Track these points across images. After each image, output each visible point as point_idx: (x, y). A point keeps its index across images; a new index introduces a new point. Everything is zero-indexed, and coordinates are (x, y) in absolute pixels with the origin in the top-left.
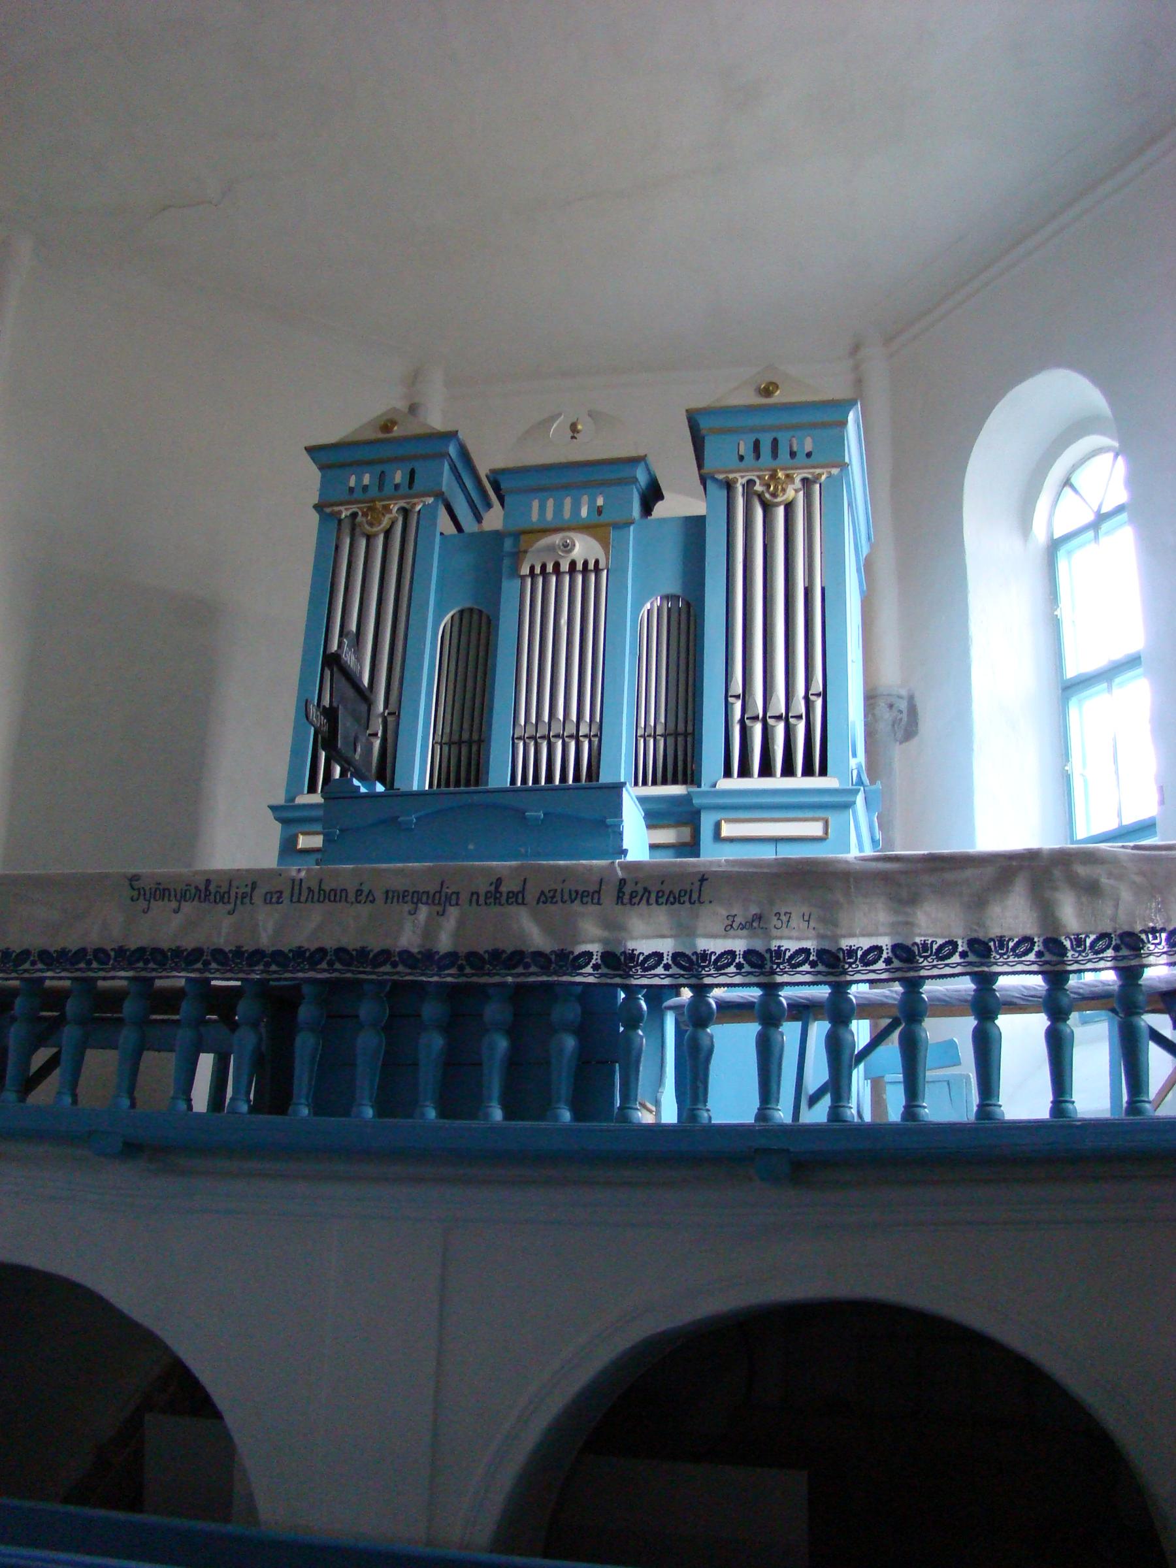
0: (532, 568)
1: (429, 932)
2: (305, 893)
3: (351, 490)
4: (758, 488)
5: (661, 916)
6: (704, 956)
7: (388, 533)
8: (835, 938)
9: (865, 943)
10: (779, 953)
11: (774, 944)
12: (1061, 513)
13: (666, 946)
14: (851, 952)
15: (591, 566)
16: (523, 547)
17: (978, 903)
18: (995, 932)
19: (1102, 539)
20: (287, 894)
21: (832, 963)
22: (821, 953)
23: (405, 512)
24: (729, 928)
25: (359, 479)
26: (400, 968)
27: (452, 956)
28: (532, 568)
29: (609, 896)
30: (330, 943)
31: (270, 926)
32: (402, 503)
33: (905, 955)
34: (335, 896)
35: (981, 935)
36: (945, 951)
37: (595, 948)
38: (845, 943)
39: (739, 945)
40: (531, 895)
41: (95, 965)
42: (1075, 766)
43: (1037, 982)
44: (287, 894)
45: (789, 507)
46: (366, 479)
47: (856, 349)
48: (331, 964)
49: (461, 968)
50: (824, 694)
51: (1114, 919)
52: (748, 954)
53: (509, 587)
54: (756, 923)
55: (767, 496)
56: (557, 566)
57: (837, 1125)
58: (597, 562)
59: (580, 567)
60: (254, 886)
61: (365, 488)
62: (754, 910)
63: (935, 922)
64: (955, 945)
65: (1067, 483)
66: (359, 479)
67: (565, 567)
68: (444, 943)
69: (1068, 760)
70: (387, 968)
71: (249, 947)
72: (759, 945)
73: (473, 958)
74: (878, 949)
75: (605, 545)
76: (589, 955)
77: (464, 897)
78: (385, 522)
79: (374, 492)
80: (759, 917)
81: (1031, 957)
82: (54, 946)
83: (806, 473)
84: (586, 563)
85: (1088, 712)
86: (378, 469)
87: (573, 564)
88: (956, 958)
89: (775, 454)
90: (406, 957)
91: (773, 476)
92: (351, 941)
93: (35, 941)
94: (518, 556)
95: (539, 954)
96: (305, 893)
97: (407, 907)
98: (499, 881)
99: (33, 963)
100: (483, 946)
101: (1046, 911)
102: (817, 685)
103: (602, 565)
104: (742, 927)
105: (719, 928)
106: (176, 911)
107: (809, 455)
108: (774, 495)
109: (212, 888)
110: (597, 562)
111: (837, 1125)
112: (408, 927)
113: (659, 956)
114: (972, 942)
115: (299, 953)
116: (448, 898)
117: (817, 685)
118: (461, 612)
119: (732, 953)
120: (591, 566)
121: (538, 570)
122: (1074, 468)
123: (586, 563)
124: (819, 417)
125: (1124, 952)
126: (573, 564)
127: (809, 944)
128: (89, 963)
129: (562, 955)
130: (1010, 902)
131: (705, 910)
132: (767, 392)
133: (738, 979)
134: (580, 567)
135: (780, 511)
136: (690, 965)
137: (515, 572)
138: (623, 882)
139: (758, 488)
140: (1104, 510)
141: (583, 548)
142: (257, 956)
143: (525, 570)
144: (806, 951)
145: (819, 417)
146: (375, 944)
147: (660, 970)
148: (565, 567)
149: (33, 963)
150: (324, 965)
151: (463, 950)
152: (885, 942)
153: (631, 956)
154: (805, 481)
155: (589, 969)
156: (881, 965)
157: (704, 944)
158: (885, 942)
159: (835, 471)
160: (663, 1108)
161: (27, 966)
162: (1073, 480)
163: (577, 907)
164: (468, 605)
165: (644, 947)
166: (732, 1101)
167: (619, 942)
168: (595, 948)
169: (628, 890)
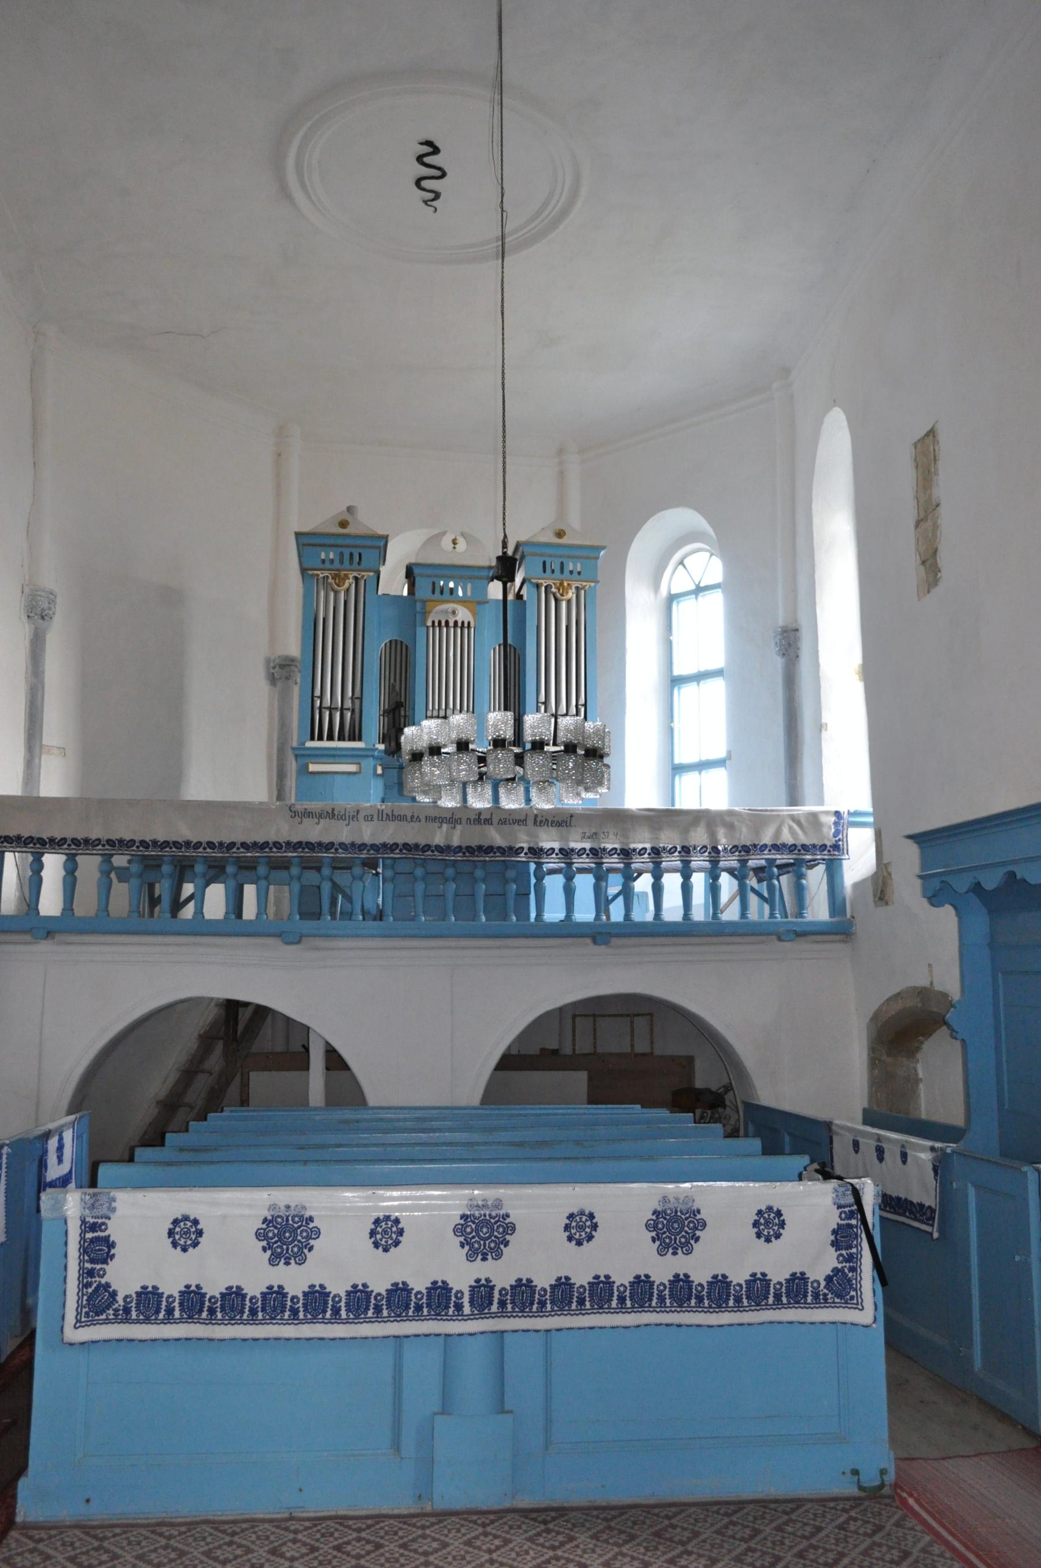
0: (433, 622)
1: (448, 836)
2: (385, 816)
3: (323, 561)
4: (554, 590)
5: (553, 831)
6: (572, 850)
7: (348, 590)
8: (628, 844)
9: (640, 846)
10: (604, 849)
11: (602, 846)
12: (678, 581)
13: (556, 845)
14: (634, 850)
15: (466, 625)
16: (428, 608)
17: (685, 831)
18: (692, 843)
19: (699, 598)
20: (375, 817)
21: (626, 854)
22: (622, 850)
23: (356, 579)
24: (584, 837)
25: (327, 555)
26: (436, 853)
27: (460, 847)
28: (433, 622)
29: (530, 822)
30: (400, 841)
31: (368, 832)
32: (355, 574)
33: (656, 851)
34: (401, 818)
35: (686, 844)
36: (671, 851)
37: (525, 845)
38: (632, 846)
39: (587, 846)
40: (495, 820)
41: (274, 850)
42: (676, 725)
43: (707, 864)
44: (375, 817)
45: (569, 602)
46: (331, 556)
47: (561, 452)
48: (401, 850)
49: (464, 853)
50: (585, 705)
51: (739, 839)
52: (591, 849)
53: (421, 631)
54: (594, 836)
55: (558, 595)
56: (447, 623)
57: (597, 922)
58: (469, 623)
59: (460, 624)
60: (358, 812)
61: (332, 561)
62: (594, 830)
63: (668, 839)
64: (676, 848)
65: (681, 563)
66: (327, 555)
67: (451, 624)
68: (456, 842)
69: (672, 721)
70: (429, 853)
71: (359, 842)
72: (596, 846)
73: (469, 849)
74: (645, 849)
75: (474, 614)
76: (522, 848)
77: (464, 821)
78: (346, 585)
79: (337, 565)
80: (596, 834)
81: (706, 854)
82: (249, 840)
83: (578, 584)
84: (463, 623)
85: (685, 694)
86: (340, 550)
87: (456, 623)
88: (677, 854)
89: (562, 571)
90: (439, 849)
91: (561, 584)
92: (411, 840)
93: (238, 837)
94: (425, 614)
95: (499, 848)
96: (385, 816)
97: (437, 825)
98: (480, 814)
99: (238, 849)
100: (474, 843)
101: (712, 835)
102: (582, 701)
103: (472, 625)
104: (589, 838)
105: (579, 837)
106: (318, 824)
107: (579, 573)
108: (562, 595)
109: (336, 812)
110: (469, 623)
111: (597, 922)
112: (438, 833)
113: (553, 849)
114: (683, 847)
115: (384, 845)
116: (456, 821)
117: (582, 701)
118: (391, 641)
119: (584, 849)
120: (466, 625)
121: (436, 624)
122: (685, 557)
123: (463, 623)
124: (584, 553)
125: (743, 853)
126: (456, 623)
127: (616, 846)
128: (271, 849)
129: (511, 848)
130: (699, 829)
131: (573, 829)
132: (560, 534)
133: (587, 860)
134: (460, 624)
135: (564, 605)
136: (566, 853)
137: (424, 623)
138: (536, 816)
139: (554, 590)
140: (702, 585)
141: (463, 615)
142: (362, 847)
143: (429, 623)
144: (616, 849)
145: (584, 553)
146: (423, 842)
147: (554, 856)
148: (451, 624)
149: (238, 849)
150: (397, 851)
151: (464, 845)
152: (648, 846)
153: (541, 849)
154: (577, 588)
155: (522, 855)
156: (646, 856)
157: (573, 845)
158: (648, 846)
159: (592, 584)
160: (554, 913)
161: (234, 850)
162: (686, 562)
163: (516, 826)
164: (395, 638)
165: (546, 845)
166: (585, 912)
167: (537, 843)
168: (525, 845)
169: (538, 820)
